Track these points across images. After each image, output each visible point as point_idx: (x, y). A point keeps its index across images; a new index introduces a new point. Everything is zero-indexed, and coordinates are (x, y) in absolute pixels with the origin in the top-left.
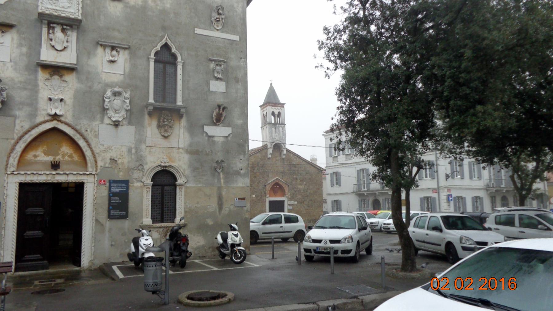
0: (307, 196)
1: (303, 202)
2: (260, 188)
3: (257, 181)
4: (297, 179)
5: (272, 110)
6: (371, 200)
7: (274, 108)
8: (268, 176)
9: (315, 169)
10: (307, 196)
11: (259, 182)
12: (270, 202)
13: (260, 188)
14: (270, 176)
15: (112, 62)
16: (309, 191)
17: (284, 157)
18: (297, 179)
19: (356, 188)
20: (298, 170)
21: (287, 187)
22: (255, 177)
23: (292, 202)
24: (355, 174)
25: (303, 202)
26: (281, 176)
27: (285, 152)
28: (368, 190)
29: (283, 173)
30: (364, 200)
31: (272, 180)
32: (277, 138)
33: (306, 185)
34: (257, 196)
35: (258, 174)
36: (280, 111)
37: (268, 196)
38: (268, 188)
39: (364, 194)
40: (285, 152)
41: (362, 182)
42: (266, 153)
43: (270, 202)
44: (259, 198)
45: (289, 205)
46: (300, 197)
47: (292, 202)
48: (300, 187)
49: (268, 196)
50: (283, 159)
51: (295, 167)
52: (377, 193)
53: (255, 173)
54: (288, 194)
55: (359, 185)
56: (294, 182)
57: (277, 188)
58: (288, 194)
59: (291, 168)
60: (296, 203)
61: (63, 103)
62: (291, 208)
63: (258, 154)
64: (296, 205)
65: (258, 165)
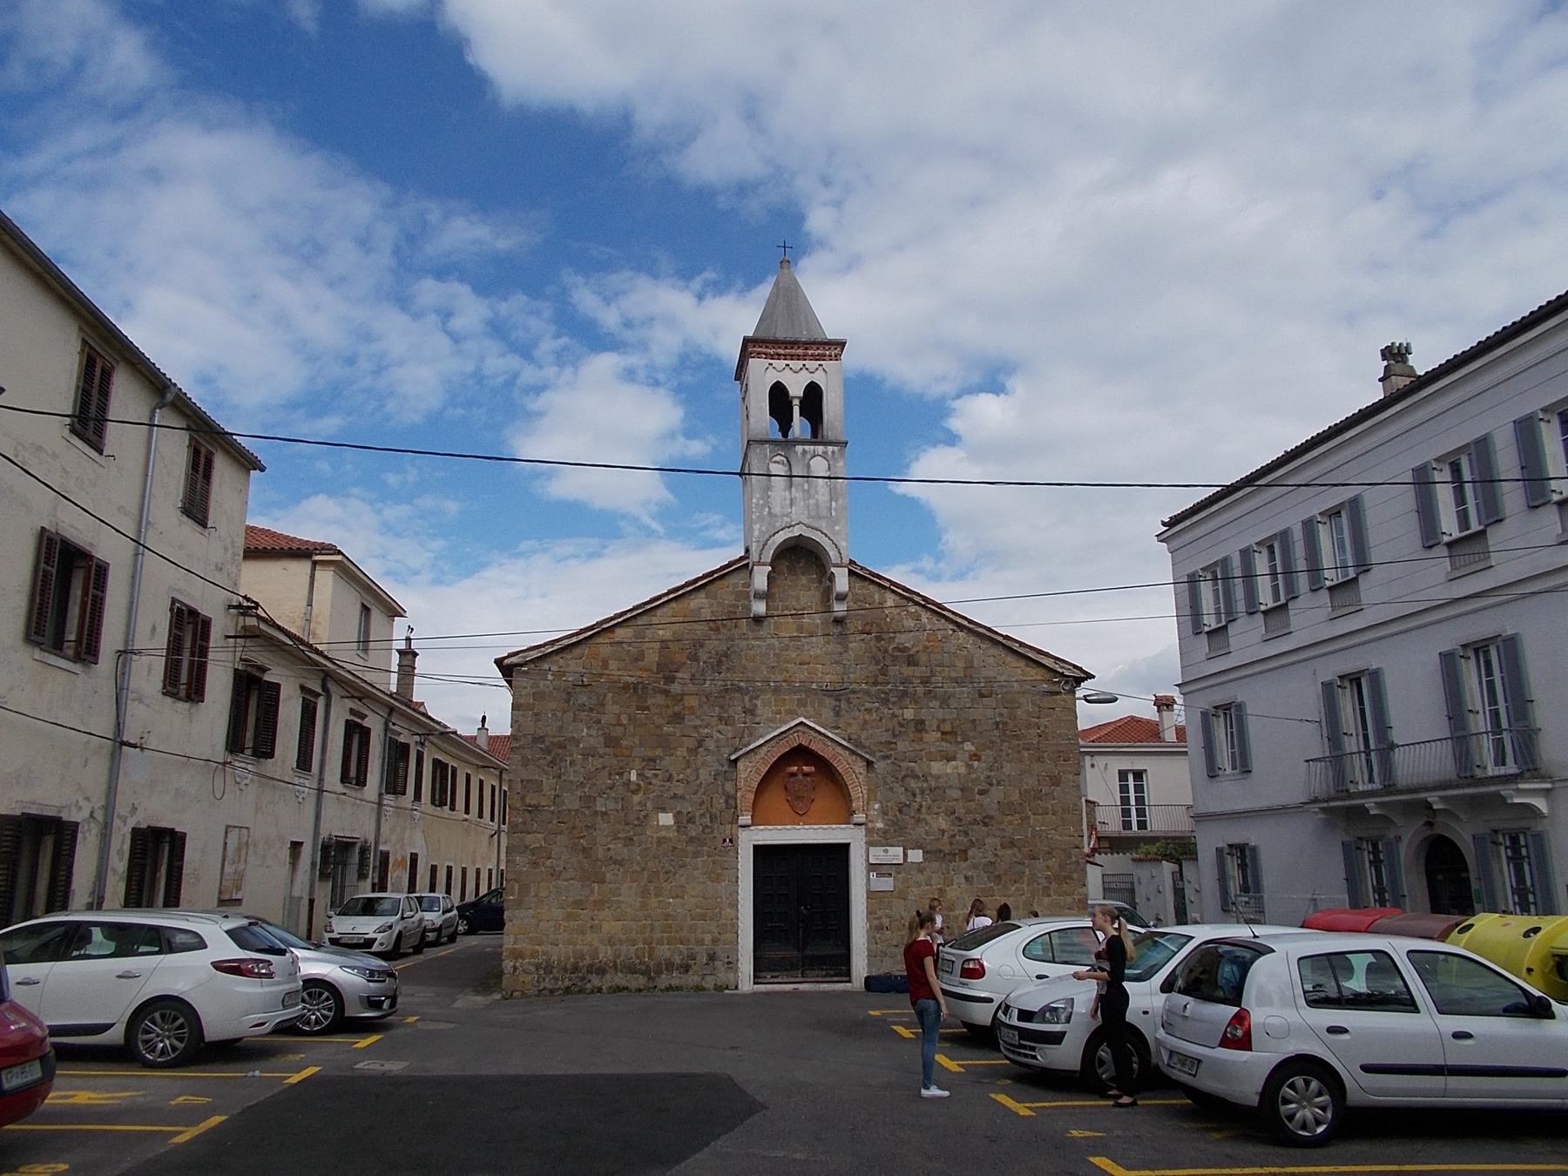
0: (986, 821)
1: (964, 855)
2: (704, 775)
3: (690, 743)
4: (920, 724)
5: (771, 378)
6: (1408, 839)
7: (781, 363)
8: (750, 712)
9: (1034, 673)
10: (986, 821)
11: (700, 743)
12: (759, 851)
13: (704, 775)
14: (764, 711)
15: (535, 863)
16: (997, 793)
17: (839, 608)
18: (920, 724)
19: (1319, 781)
20: (925, 681)
21: (860, 767)
22: (677, 718)
23: (895, 854)
24: (1313, 706)
25: (964, 855)
26: (827, 714)
27: (842, 583)
28: (1389, 789)
29: (837, 694)
30: (1138, 775)
31: (772, 731)
32: (798, 513)
33: (975, 757)
34: (683, 821)
35: (692, 701)
36: (819, 378)
37: (745, 819)
38: (750, 773)
39: (1363, 810)
40: (842, 583)
41: (1352, 744)
42: (745, 595)
43: (759, 851)
44: (694, 831)
45: (872, 867)
46: (942, 822)
47: (895, 854)
48: (937, 767)
49: (745, 819)
50: (838, 621)
51: (912, 661)
52: (1432, 797)
53: (680, 698)
54: (867, 808)
55: (1336, 759)
56: (902, 745)
57: (803, 772)
58: (867, 808)
59: (884, 671)
60: (916, 856)
61: (837, 630)
62: (887, 884)
63: (699, 601)
64: (920, 868)
65: (694, 658)
